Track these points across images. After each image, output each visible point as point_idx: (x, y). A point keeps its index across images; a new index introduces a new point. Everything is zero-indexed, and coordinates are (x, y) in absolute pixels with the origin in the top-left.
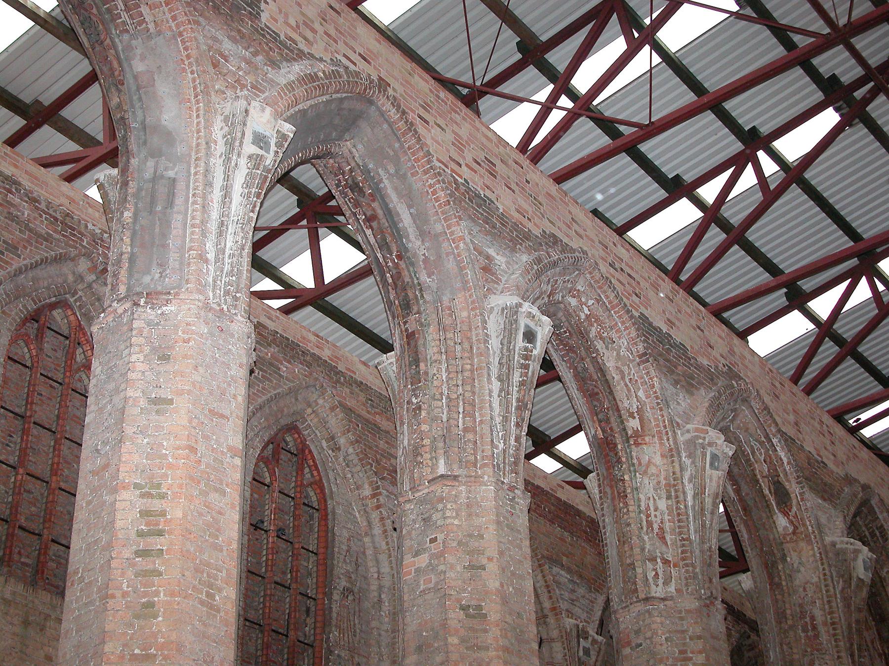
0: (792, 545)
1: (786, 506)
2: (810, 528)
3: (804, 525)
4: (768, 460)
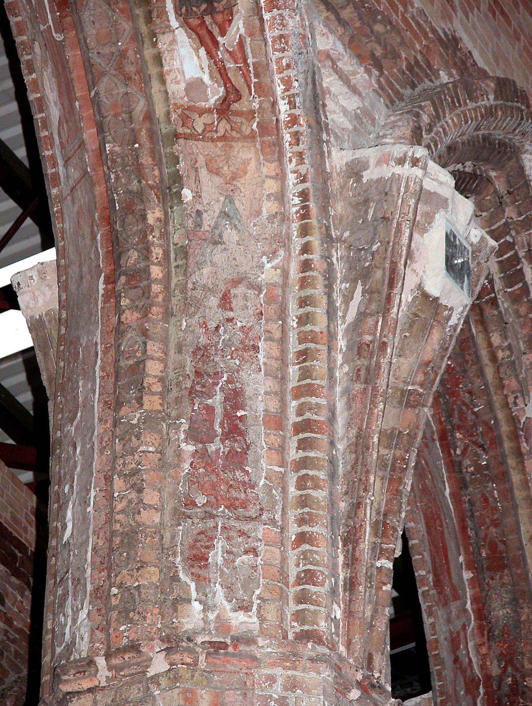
0: (214, 149)
1: (211, 11)
2: (283, 106)
3: (264, 90)
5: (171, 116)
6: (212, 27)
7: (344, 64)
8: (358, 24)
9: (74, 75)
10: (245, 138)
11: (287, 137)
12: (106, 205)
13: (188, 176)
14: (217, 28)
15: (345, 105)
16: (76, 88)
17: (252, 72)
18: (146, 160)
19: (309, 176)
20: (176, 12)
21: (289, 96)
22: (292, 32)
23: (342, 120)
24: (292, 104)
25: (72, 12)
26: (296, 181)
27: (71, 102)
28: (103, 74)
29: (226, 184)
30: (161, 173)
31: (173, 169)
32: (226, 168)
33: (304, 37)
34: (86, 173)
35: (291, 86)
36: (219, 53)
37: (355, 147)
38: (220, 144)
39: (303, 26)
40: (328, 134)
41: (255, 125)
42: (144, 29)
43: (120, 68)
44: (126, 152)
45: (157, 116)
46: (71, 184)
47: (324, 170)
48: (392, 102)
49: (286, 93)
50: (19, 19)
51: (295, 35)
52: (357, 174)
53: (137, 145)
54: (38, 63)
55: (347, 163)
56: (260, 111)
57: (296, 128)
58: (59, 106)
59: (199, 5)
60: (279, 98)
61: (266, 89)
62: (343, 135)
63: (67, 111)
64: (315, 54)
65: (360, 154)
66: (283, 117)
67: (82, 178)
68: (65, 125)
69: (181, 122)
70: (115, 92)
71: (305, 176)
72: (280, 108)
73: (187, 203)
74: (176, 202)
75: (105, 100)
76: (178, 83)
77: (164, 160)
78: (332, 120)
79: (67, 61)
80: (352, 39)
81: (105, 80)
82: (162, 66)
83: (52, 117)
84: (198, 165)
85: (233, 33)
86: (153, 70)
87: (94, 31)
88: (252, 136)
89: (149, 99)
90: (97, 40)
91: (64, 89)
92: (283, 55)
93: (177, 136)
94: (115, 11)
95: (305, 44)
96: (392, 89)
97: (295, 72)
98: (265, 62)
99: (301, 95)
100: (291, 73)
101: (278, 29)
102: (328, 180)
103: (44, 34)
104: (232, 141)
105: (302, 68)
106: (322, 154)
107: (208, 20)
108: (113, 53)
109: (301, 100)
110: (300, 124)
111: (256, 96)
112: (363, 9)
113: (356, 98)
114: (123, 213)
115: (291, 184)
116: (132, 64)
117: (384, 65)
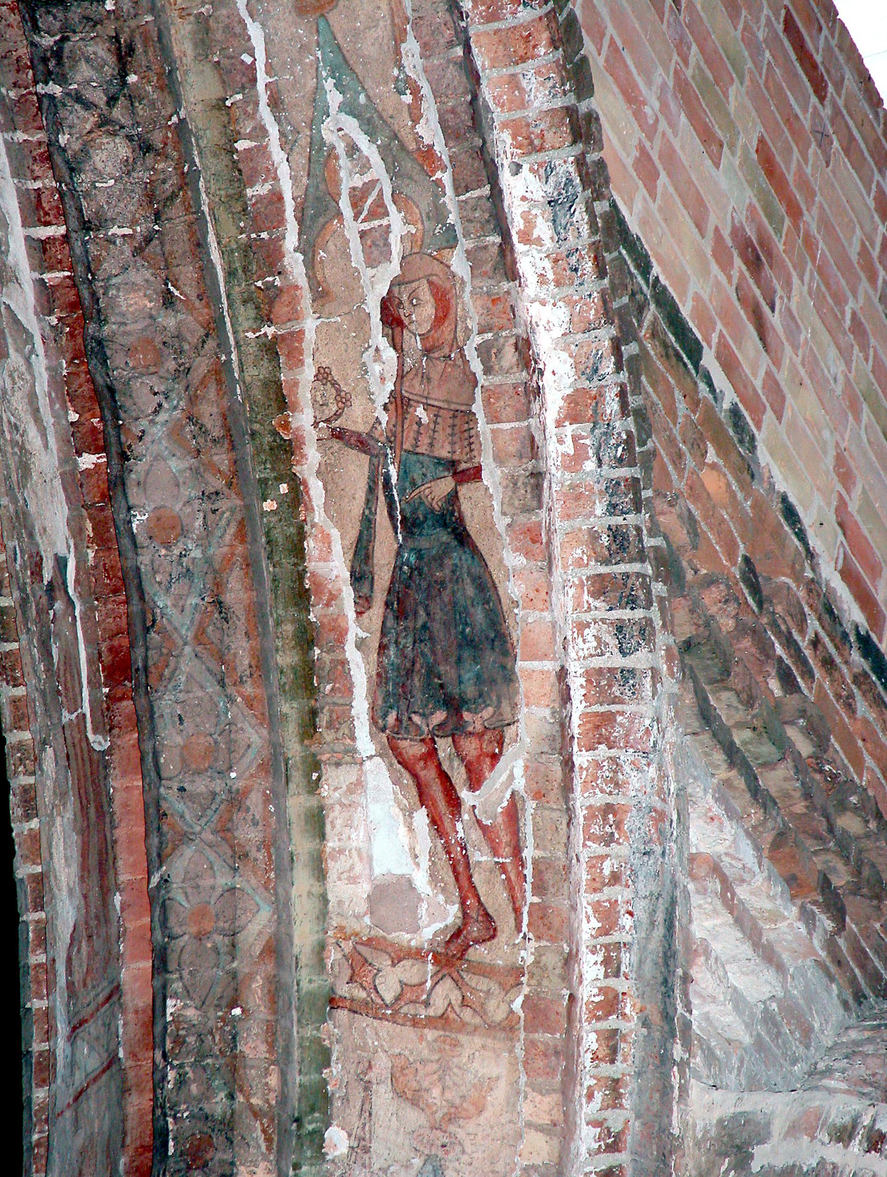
0: (414, 1044)
1: (455, 729)
2: (590, 969)
3: (549, 924)
4: (422, 315)
5: (325, 954)
6: (452, 767)
7: (752, 893)
8: (800, 807)
9: (120, 833)
10: (491, 1028)
11: (590, 1041)
12: (148, 1140)
13: (346, 1099)
14: (463, 770)
15: (741, 987)
16: (120, 863)
17: (530, 879)
18: (253, 1047)
19: (629, 1138)
20: (373, 721)
21: (607, 947)
22: (634, 802)
23: (728, 1019)
24: (612, 967)
25: (135, 689)
26: (596, 1146)
27: (105, 893)
28: (185, 838)
29: (431, 1128)
30: (284, 1081)
31: (314, 1077)
32: (436, 1092)
33: (661, 816)
34: (113, 1061)
35: (616, 923)
36: (459, 826)
37: (753, 1085)
38: (430, 1034)
39: (662, 793)
40: (687, 1046)
41: (519, 1000)
42: (294, 749)
43: (225, 830)
44: (210, 1024)
45: (296, 950)
46: (77, 1083)
47: (665, 1130)
48: (859, 997)
49: (603, 940)
50: (20, 691)
51: (639, 810)
52: (739, 1148)
53: (237, 1011)
54: (46, 797)
55: (720, 1121)
56: (535, 970)
57: (613, 1022)
58: (78, 900)
59: (427, 712)
60: (583, 949)
61: (556, 922)
62: (728, 1055)
63: (93, 910)
64: (681, 860)
65: (755, 1103)
66: (588, 993)
67: (104, 1071)
68: (84, 944)
69: (349, 972)
70: (206, 882)
71: (618, 1137)
72: (584, 971)
73: (333, 1161)
74: (309, 1154)
75: (180, 898)
76: (354, 880)
77: (296, 1054)
78: (707, 1017)
79: (111, 800)
80: (781, 838)
81: (189, 851)
82: (322, 836)
83: (59, 923)
84: (372, 1076)
85: (497, 786)
86: (301, 844)
87: (179, 740)
88: (509, 1027)
89: (282, 910)
90: (183, 760)
91: (93, 861)
92: (607, 850)
93: (333, 1002)
94: (232, 700)
95: (661, 832)
96: (862, 967)
97: (628, 894)
98: (563, 861)
99: (635, 947)
100: (620, 894)
101: (602, 791)
102: (671, 1153)
103: (68, 733)
104: (460, 1031)
105: (645, 886)
106: (665, 1090)
107: (444, 747)
108: (214, 795)
109: (635, 959)
110: (624, 1015)
111: (531, 935)
112: (818, 777)
113: (770, 974)
114: (183, 1165)
115: (583, 1150)
116: (255, 823)
117: (849, 909)
